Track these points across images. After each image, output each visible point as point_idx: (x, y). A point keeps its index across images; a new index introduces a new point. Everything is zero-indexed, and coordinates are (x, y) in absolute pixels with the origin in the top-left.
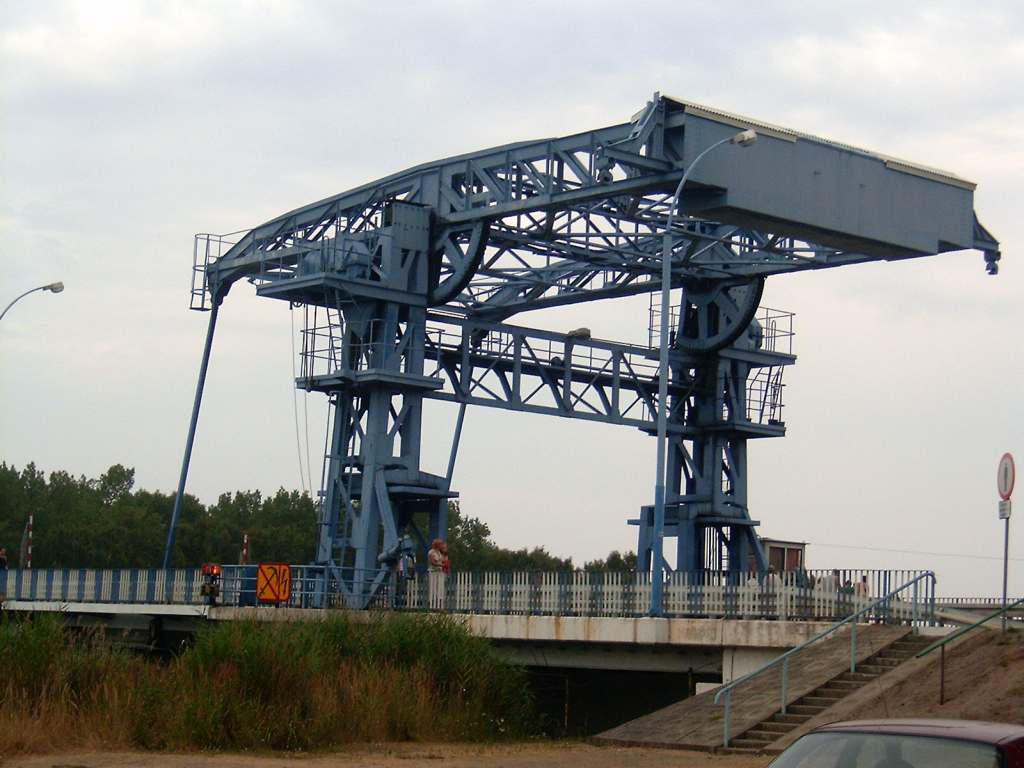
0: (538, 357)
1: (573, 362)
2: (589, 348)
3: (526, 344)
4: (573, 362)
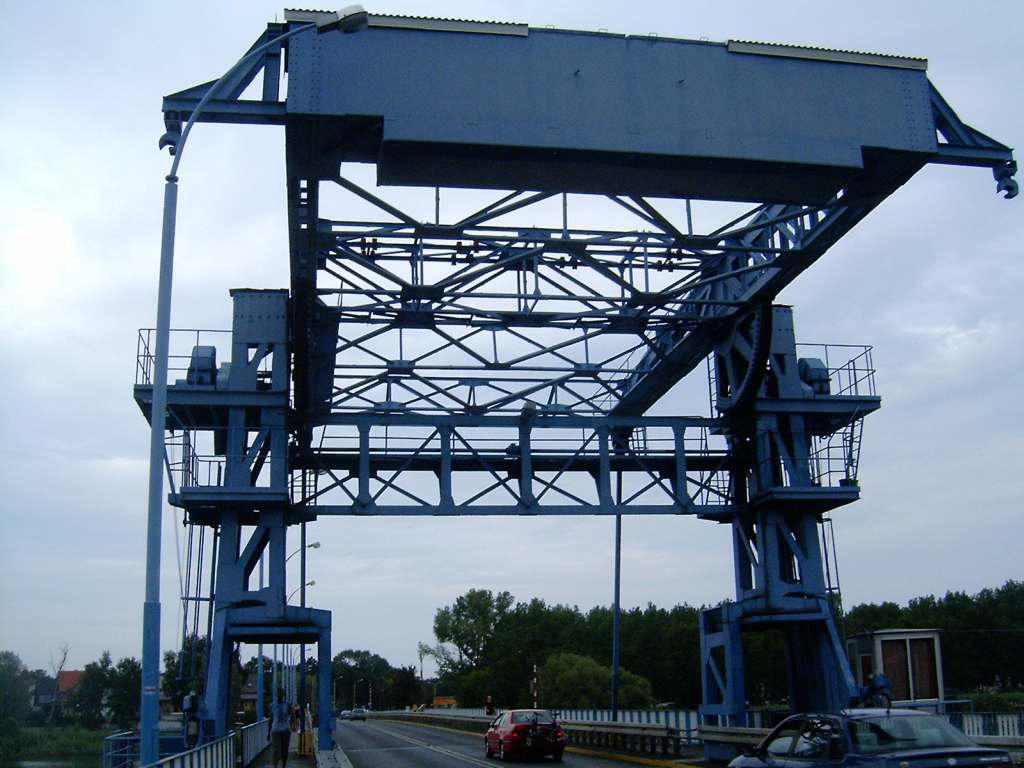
3: (456, 434)
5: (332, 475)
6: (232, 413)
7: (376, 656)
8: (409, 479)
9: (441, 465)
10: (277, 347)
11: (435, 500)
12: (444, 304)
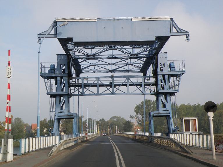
5: (116, 88)
6: (165, 76)
7: (122, 118)
8: (91, 88)
10: (66, 65)
11: (96, 92)
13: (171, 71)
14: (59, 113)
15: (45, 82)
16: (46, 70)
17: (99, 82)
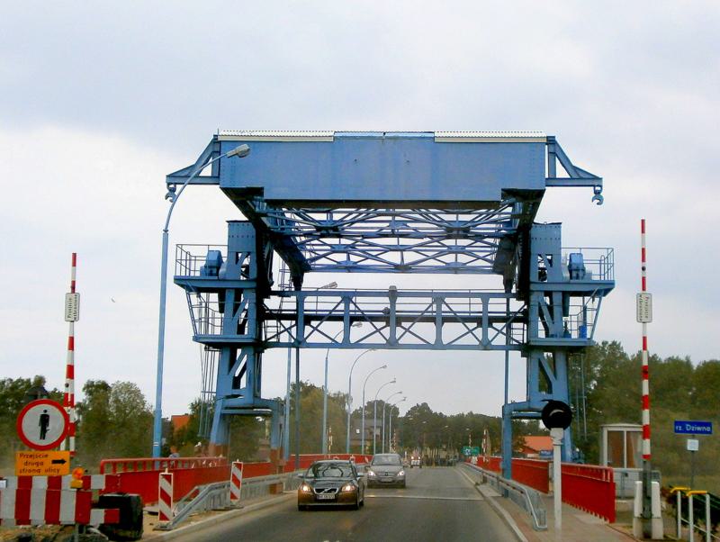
0: (362, 309)
1: (305, 308)
2: (581, 298)
4: (305, 308)
6: (227, 293)
8: (327, 326)
9: (439, 320)
11: (340, 339)
12: (357, 241)
13: (572, 281)
14: (228, 397)
15: (190, 302)
16: (197, 269)
17: (444, 308)
